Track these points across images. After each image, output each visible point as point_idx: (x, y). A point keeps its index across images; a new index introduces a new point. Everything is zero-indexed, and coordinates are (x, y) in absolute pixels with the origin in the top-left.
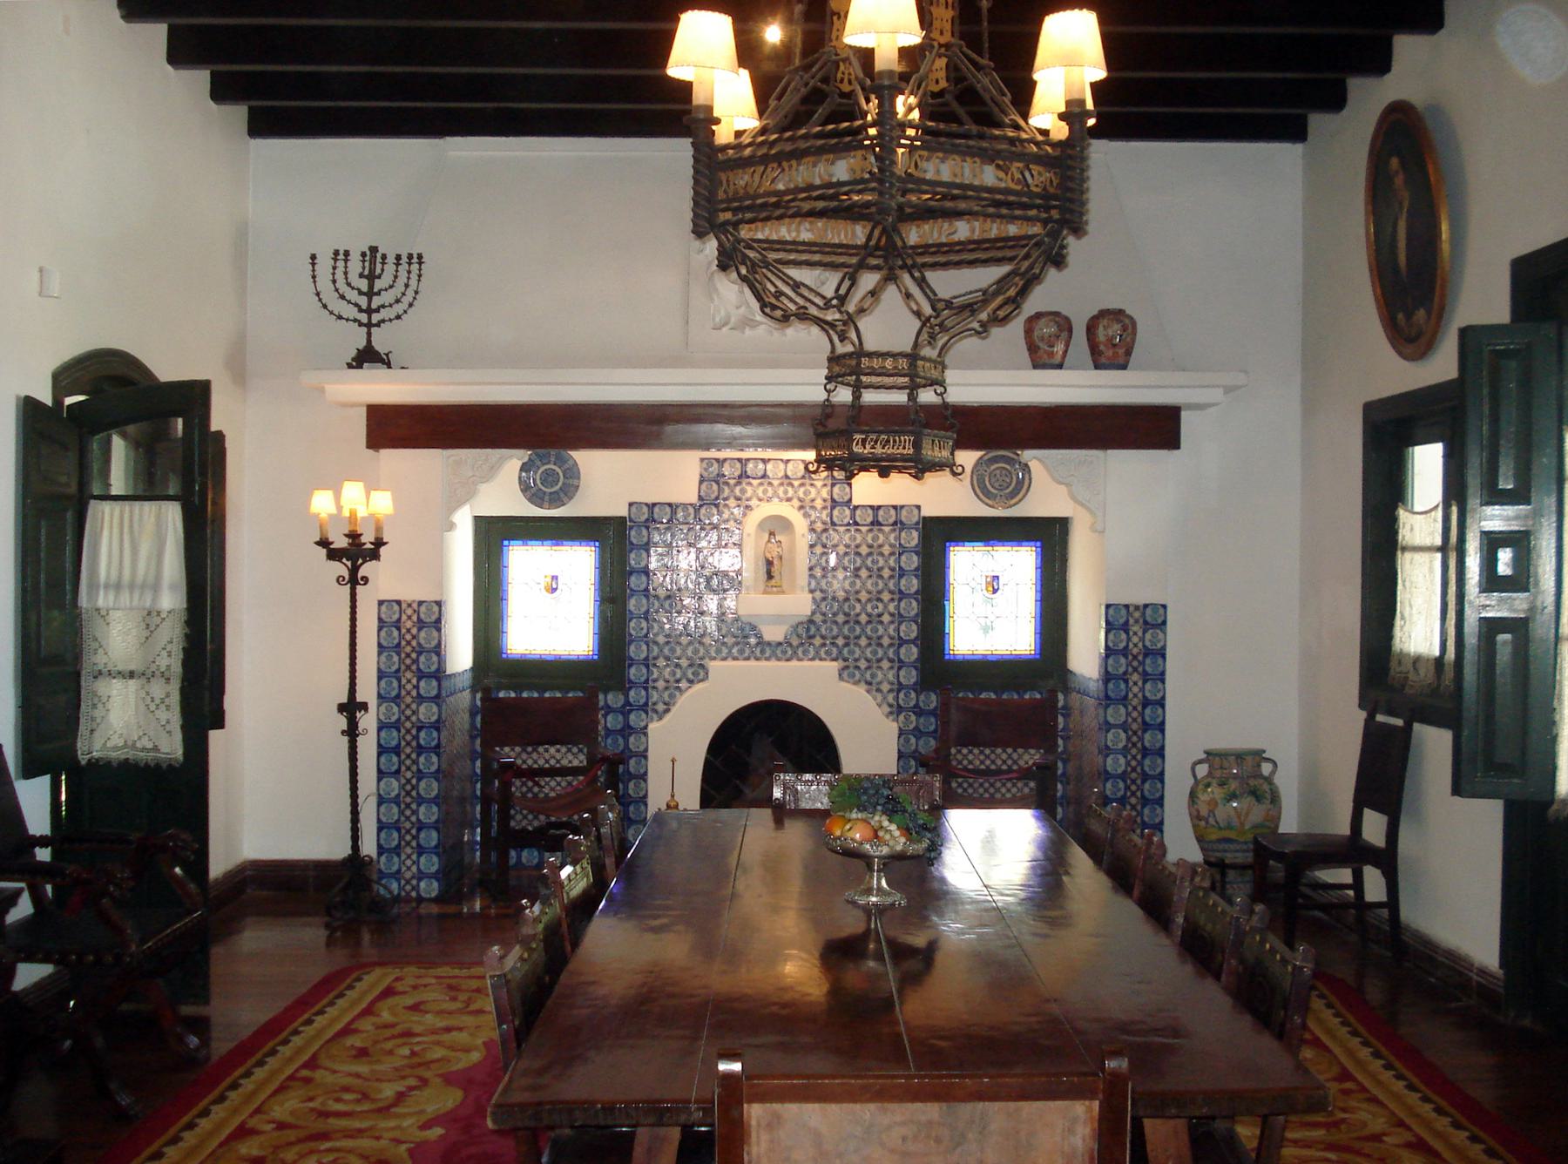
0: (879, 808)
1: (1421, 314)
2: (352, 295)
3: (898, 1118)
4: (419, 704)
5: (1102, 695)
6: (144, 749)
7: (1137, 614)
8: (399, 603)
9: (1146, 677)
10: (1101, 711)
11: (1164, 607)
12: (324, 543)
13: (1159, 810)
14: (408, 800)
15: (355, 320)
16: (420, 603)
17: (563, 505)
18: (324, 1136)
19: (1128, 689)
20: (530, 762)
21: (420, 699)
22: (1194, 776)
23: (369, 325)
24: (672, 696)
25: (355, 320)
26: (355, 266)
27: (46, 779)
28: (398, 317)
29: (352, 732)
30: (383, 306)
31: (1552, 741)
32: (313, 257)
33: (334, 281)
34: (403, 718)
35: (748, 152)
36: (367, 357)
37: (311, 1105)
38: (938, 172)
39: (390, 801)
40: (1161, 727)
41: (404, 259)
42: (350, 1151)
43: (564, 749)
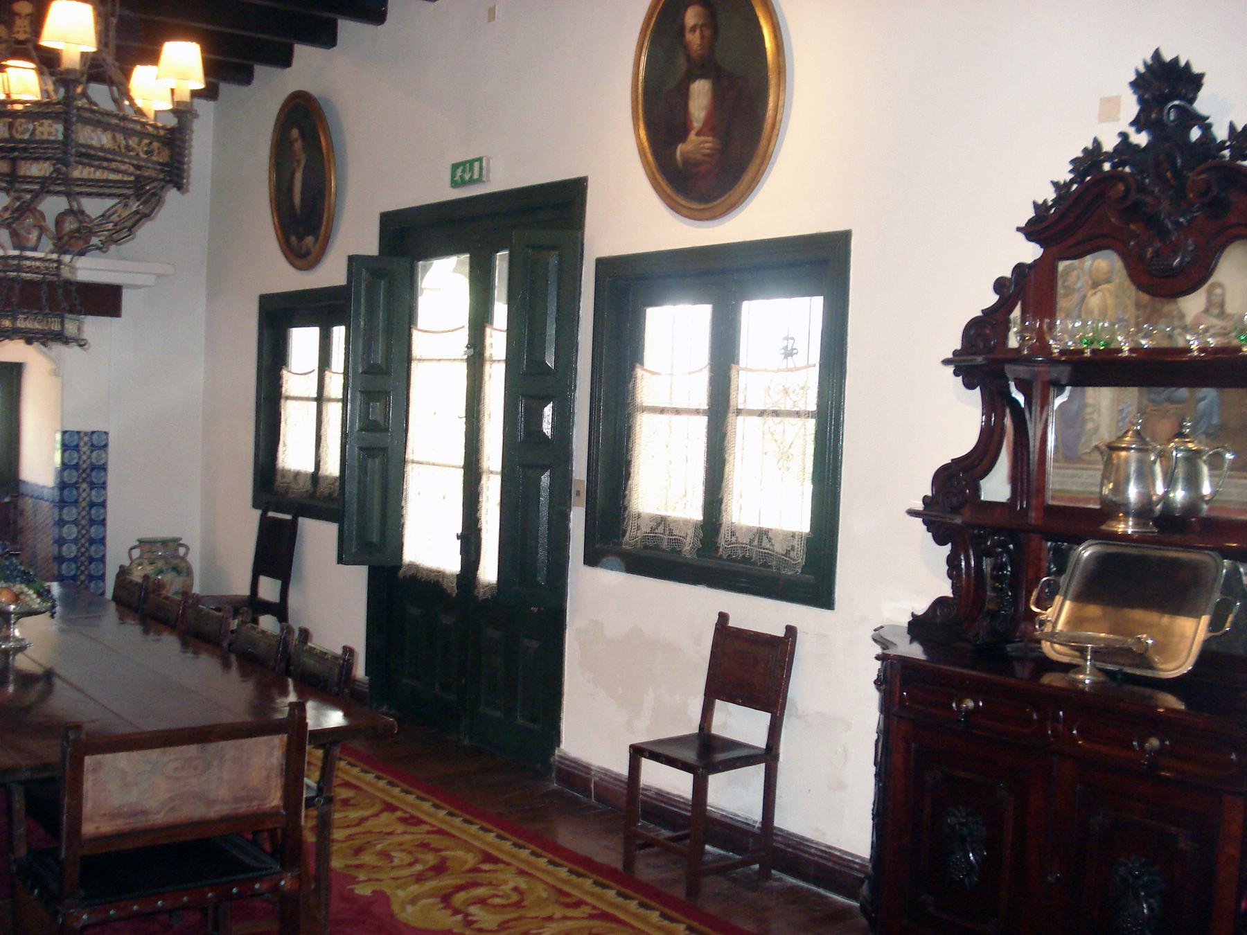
0: (18, 579)
1: (309, 240)
3: (172, 757)
5: (57, 499)
7: (86, 439)
9: (92, 486)
10: (56, 511)
11: (106, 433)
13: (101, 584)
19: (79, 495)
22: (130, 557)
31: (400, 527)
38: (100, 140)
40: (103, 523)
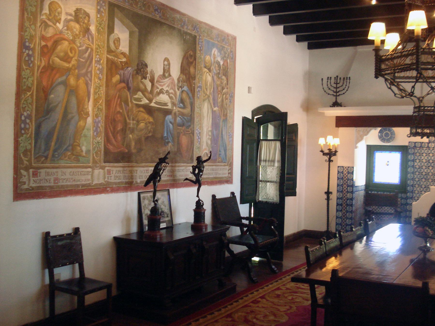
2: (332, 89)
4: (348, 193)
6: (270, 199)
8: (343, 167)
12: (322, 151)
14: (344, 218)
15: (333, 95)
16: (349, 167)
17: (390, 142)
18: (296, 292)
20: (380, 211)
21: (348, 192)
23: (336, 96)
24: (420, 196)
25: (333, 95)
26: (333, 80)
27: (248, 204)
28: (344, 94)
29: (328, 199)
30: (340, 91)
32: (322, 79)
33: (327, 85)
34: (343, 197)
35: (410, 52)
36: (336, 104)
37: (297, 286)
39: (339, 218)
41: (346, 79)
42: (300, 296)
43: (389, 208)
